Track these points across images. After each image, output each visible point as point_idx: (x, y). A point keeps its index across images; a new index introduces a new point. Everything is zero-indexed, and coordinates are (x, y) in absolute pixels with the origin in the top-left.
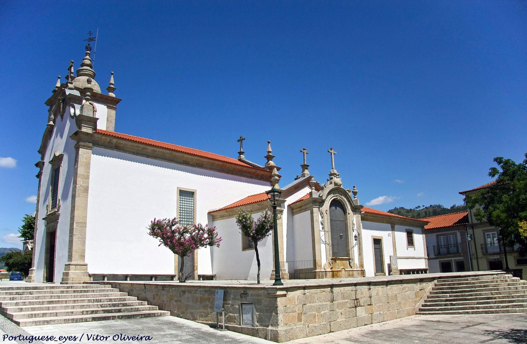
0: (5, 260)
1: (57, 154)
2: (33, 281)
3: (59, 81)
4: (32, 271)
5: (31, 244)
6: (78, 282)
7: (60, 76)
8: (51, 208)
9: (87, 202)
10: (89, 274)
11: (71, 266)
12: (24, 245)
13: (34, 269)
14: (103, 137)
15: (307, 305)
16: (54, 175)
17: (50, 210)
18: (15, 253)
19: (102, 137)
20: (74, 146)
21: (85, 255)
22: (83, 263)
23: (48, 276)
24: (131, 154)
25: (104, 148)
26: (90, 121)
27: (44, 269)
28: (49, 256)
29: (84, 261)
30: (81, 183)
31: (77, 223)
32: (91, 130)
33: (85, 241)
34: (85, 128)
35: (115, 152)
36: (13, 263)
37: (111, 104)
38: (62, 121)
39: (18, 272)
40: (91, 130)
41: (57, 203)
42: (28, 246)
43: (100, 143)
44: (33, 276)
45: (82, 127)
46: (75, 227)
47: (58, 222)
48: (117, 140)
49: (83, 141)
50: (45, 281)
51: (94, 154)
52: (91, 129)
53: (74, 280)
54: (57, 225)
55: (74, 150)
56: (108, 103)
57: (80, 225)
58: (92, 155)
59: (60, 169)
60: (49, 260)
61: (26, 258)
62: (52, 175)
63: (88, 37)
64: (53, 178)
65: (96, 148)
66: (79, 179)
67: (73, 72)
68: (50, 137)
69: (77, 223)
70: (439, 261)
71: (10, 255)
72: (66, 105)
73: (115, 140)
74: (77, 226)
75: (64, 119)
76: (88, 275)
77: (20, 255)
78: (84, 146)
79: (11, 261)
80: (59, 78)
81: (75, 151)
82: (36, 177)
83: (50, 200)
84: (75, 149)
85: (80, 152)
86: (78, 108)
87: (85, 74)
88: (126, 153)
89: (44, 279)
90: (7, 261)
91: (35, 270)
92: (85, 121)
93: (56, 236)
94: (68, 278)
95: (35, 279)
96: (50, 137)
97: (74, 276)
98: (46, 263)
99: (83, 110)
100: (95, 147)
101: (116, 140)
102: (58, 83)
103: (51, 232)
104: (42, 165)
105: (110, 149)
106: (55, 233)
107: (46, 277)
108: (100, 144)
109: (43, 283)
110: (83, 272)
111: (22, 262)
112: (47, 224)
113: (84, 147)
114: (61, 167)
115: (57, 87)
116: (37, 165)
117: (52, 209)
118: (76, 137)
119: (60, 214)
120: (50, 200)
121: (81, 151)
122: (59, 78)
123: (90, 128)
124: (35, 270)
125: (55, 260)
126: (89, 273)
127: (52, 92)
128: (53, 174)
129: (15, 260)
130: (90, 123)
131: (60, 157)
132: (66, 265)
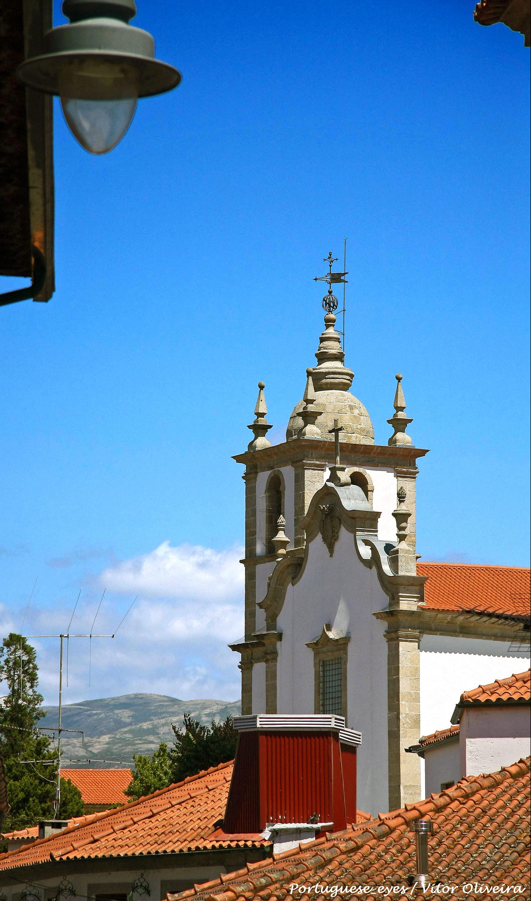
14: (440, 616)
19: (437, 615)
24: (490, 639)
25: (441, 634)
32: (415, 601)
34: (405, 599)
35: (462, 640)
37: (403, 466)
38: (331, 556)
40: (415, 601)
45: (400, 599)
52: (416, 600)
55: (384, 646)
56: (397, 465)
57: (410, 792)
58: (420, 653)
63: (324, 271)
65: (427, 638)
66: (403, 703)
69: (405, 787)
70: (91, 887)
72: (341, 523)
75: (335, 554)
78: (407, 637)
81: (387, 643)
84: (385, 640)
85: (401, 649)
86: (386, 564)
87: (331, 384)
88: (481, 638)
99: (399, 564)
100: (425, 636)
105: (452, 636)
108: (433, 628)
113: (408, 638)
121: (404, 647)
123: (414, 597)
128: (319, 670)
130: (413, 588)
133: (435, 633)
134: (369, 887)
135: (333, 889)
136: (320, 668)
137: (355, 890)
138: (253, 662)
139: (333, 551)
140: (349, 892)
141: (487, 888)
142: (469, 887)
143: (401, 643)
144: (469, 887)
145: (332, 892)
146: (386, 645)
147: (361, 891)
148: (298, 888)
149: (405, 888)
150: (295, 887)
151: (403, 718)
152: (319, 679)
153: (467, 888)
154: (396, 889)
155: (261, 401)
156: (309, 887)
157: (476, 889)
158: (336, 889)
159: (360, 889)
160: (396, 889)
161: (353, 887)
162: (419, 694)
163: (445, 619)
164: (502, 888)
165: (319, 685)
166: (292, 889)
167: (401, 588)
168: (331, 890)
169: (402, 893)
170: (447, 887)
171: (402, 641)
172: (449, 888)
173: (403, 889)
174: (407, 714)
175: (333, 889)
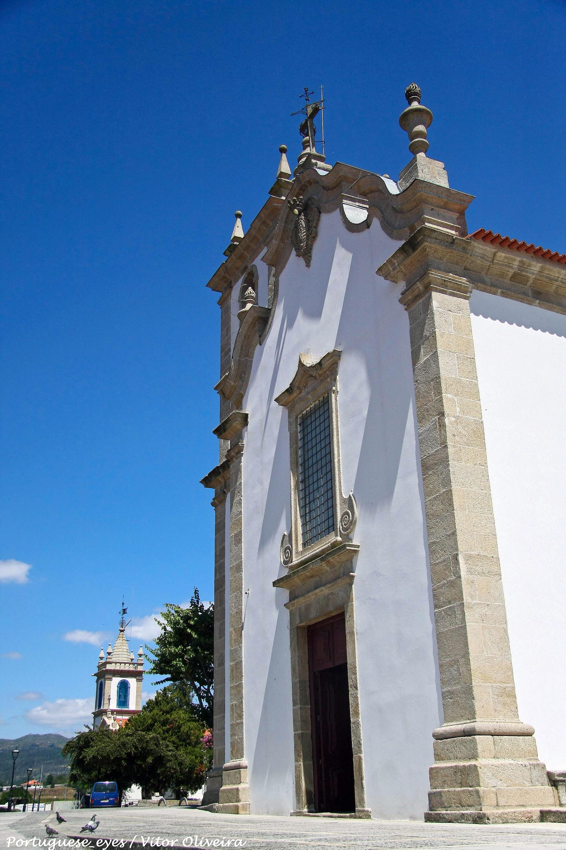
0: (73, 751)
1: (310, 360)
2: (245, 808)
3: (239, 222)
4: (240, 772)
5: (112, 717)
6: (523, 814)
7: (240, 212)
8: (300, 542)
9: (488, 480)
10: (550, 775)
11: (477, 737)
12: (94, 718)
13: (244, 765)
15: (497, 844)
16: (300, 436)
17: (300, 548)
18: (98, 733)
19: (495, 254)
20: (400, 296)
21: (514, 688)
22: (511, 726)
23: (312, 789)
25: (504, 295)
26: (445, 207)
27: (297, 761)
28: (309, 712)
29: (516, 714)
30: (458, 409)
31: (469, 558)
33: (506, 631)
36: (94, 757)
39: (107, 782)
41: (334, 515)
42: (106, 719)
43: (487, 279)
44: (244, 789)
46: (463, 573)
47: (353, 577)
48: (542, 268)
49: (439, 269)
50: (306, 810)
51: (477, 314)
53: (502, 801)
54: (351, 589)
58: (472, 315)
59: (333, 401)
60: (310, 726)
61: (124, 744)
62: (293, 440)
64: (297, 443)
65: (477, 294)
67: (291, 174)
68: (260, 336)
69: (469, 558)
71: (87, 738)
73: (536, 266)
74: (470, 571)
76: (546, 780)
77: (109, 737)
79: (89, 753)
80: (239, 216)
82: (202, 486)
83: (296, 517)
84: (401, 307)
89: (299, 800)
90: (80, 754)
91: (246, 767)
92: (432, 204)
93: (352, 633)
94: (477, 792)
95: (250, 801)
96: (260, 336)
97: (502, 786)
98: (300, 738)
101: (540, 265)
102: (236, 228)
103: (309, 627)
104: (239, 427)
105: (517, 299)
106: (343, 621)
107: (308, 793)
109: (299, 814)
110: (527, 763)
111: (117, 754)
112: (290, 601)
114: (333, 395)
115: (236, 239)
116: (220, 431)
117: (304, 545)
118: (408, 261)
119: (358, 547)
120: (296, 517)
122: (239, 216)
124: (246, 767)
125: (358, 725)
126: (549, 769)
127: (224, 254)
128: (297, 431)
129: (99, 749)
131: (326, 365)
132: (439, 737)
133: (494, 289)
134: (219, 841)
135: (51, 843)
136: (297, 428)
137: (73, 844)
138: (226, 492)
139: (311, 257)
140: (47, 845)
141: (207, 841)
142: (189, 840)
143: (434, 294)
144: (189, 840)
145: (50, 845)
146: (406, 314)
147: (79, 844)
148: (16, 841)
149: (207, 845)
150: (12, 840)
151: (451, 423)
152: (297, 443)
153: (187, 841)
154: (216, 842)
155: (238, 227)
156: (173, 841)
157: (196, 843)
158: (54, 843)
159: (79, 843)
160: (216, 842)
161: (78, 847)
162: (476, 385)
163: (509, 267)
164: (223, 842)
165: (297, 453)
166: (9, 843)
167: (427, 208)
168: (49, 844)
169: (120, 846)
170: (167, 840)
171: (437, 290)
172: (168, 841)
173: (122, 843)
174: (457, 418)
175: (51, 843)
